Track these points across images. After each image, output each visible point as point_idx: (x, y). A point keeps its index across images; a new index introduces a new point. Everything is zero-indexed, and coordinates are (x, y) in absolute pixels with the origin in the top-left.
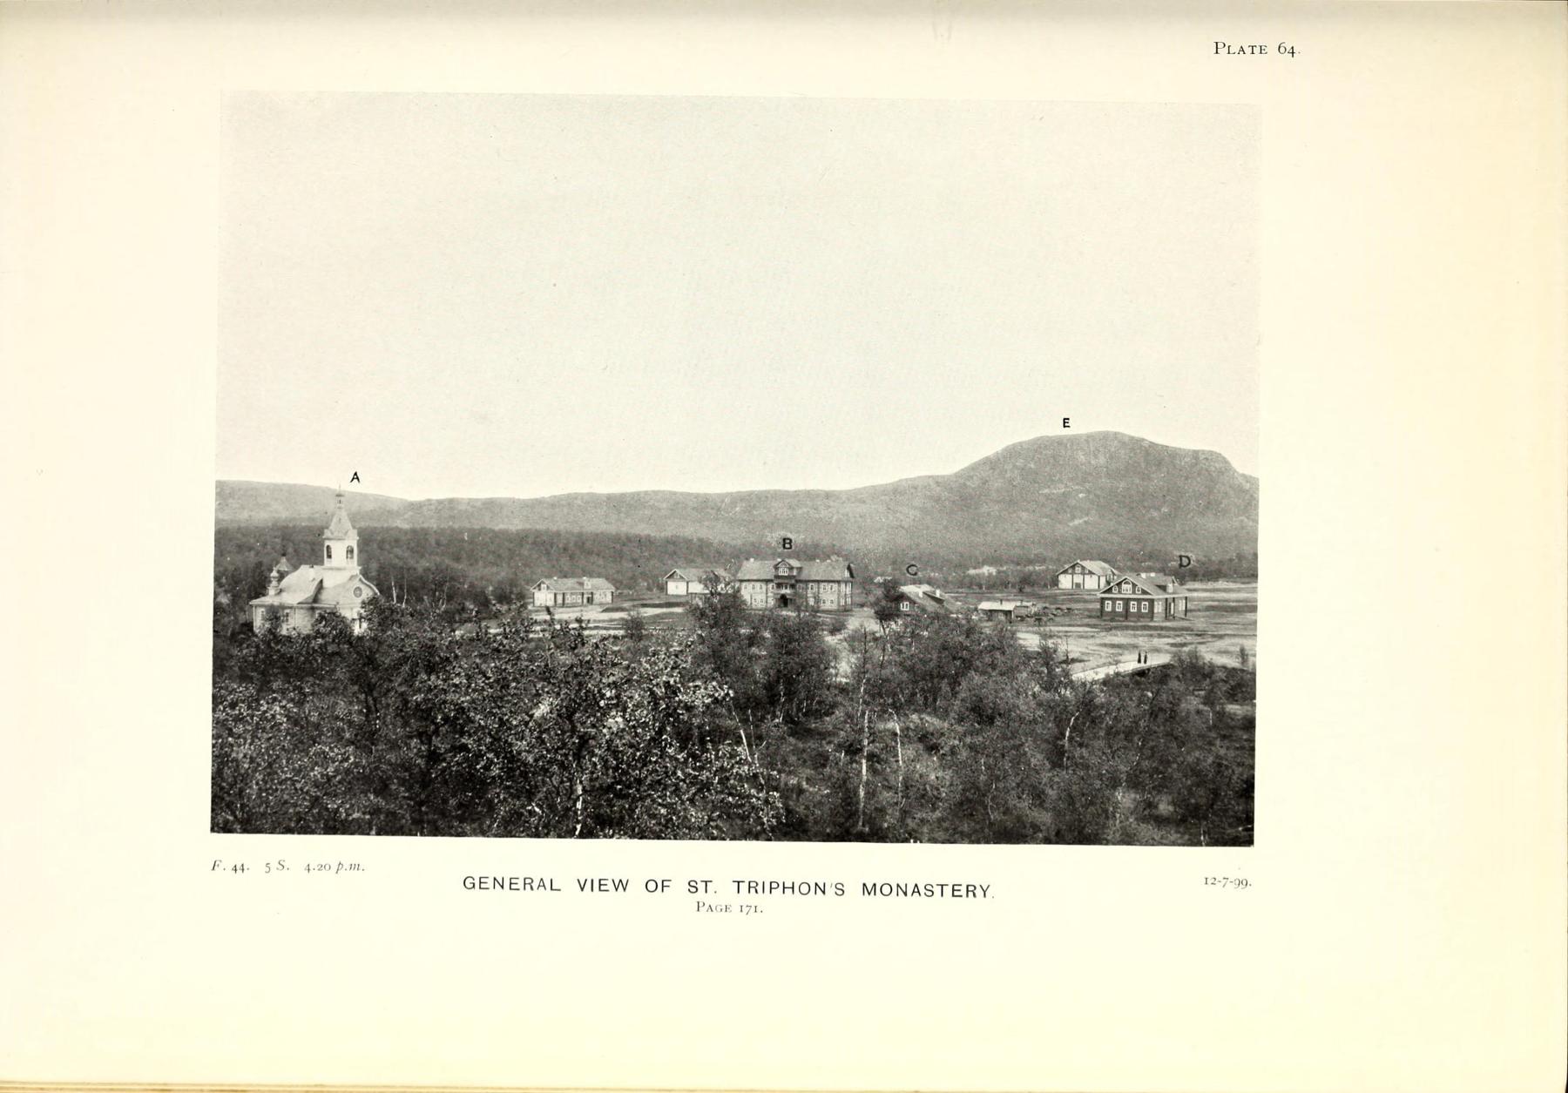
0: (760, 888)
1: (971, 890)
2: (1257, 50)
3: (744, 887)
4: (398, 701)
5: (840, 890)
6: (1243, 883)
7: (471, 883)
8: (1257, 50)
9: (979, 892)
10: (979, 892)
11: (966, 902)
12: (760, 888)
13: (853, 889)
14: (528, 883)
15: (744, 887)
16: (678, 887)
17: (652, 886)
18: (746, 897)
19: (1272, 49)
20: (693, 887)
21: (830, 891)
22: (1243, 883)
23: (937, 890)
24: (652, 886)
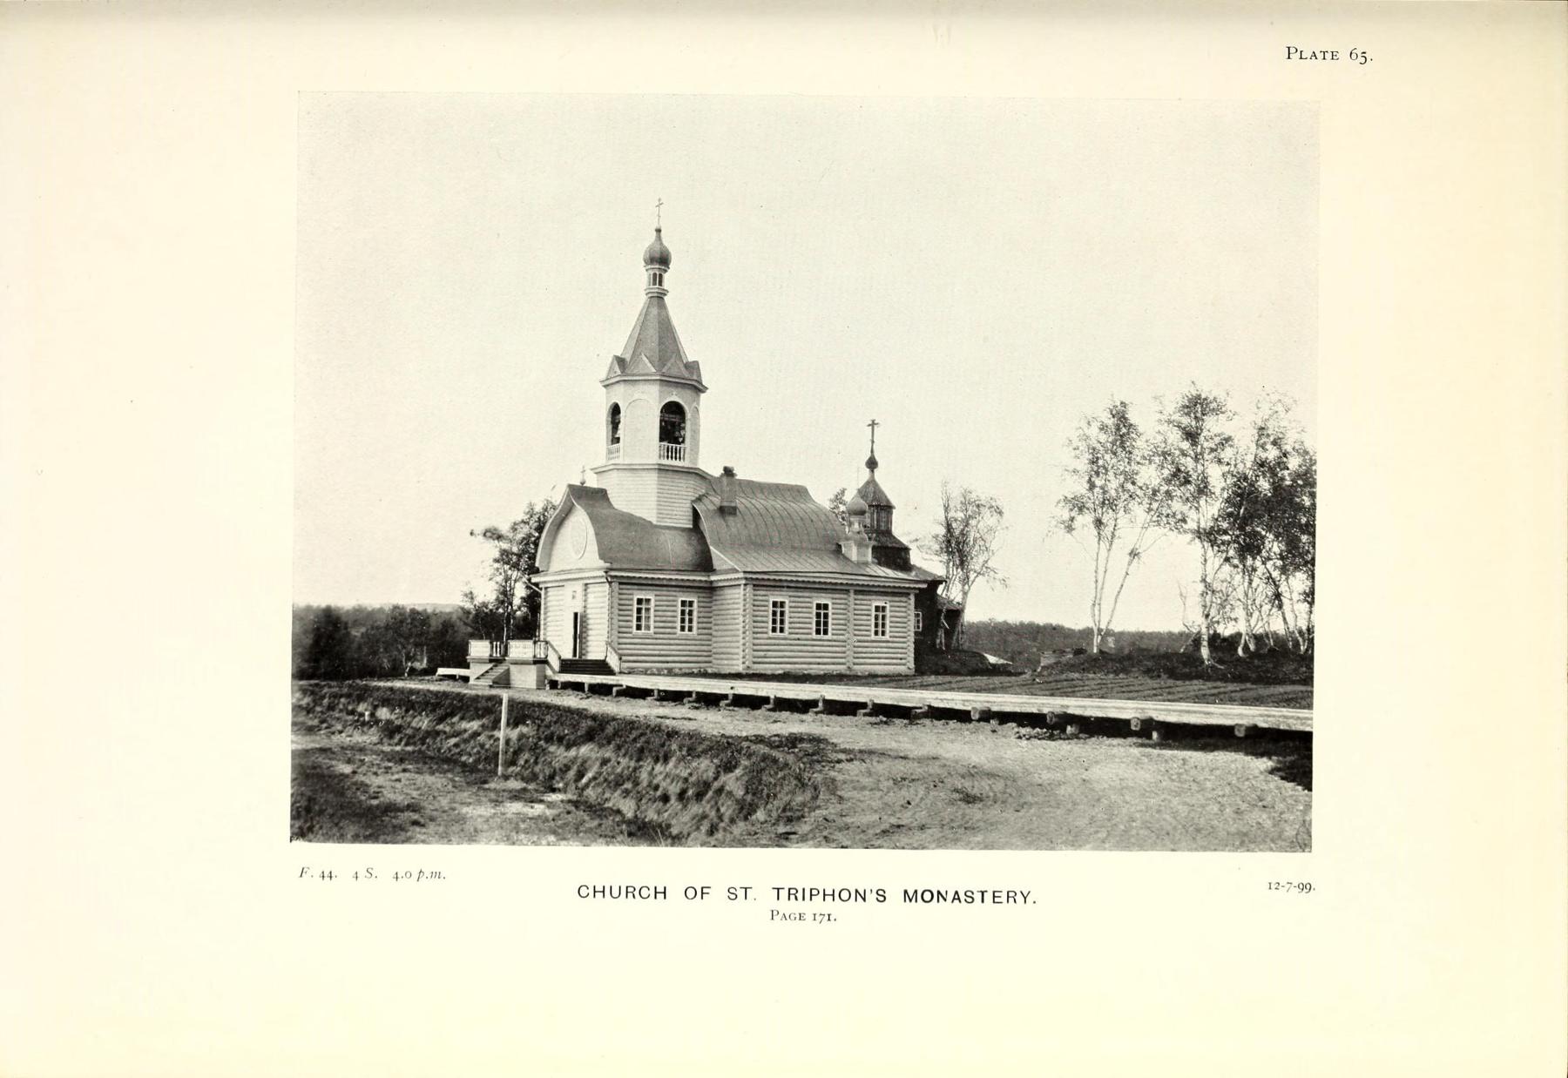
0: (800, 895)
1: (615, 424)
2: (1328, 56)
3: (784, 894)
4: (396, 714)
5: (882, 896)
6: (1306, 887)
7: (1275, 886)
8: (1328, 56)
9: (1019, 898)
10: (1019, 898)
11: (1006, 908)
12: (800, 895)
13: (895, 895)
14: (630, 891)
15: (784, 894)
16: (718, 894)
17: (691, 893)
18: (786, 906)
19: (1343, 55)
20: (732, 894)
21: (871, 897)
22: (1306, 887)
23: (978, 897)
24: (691, 893)
